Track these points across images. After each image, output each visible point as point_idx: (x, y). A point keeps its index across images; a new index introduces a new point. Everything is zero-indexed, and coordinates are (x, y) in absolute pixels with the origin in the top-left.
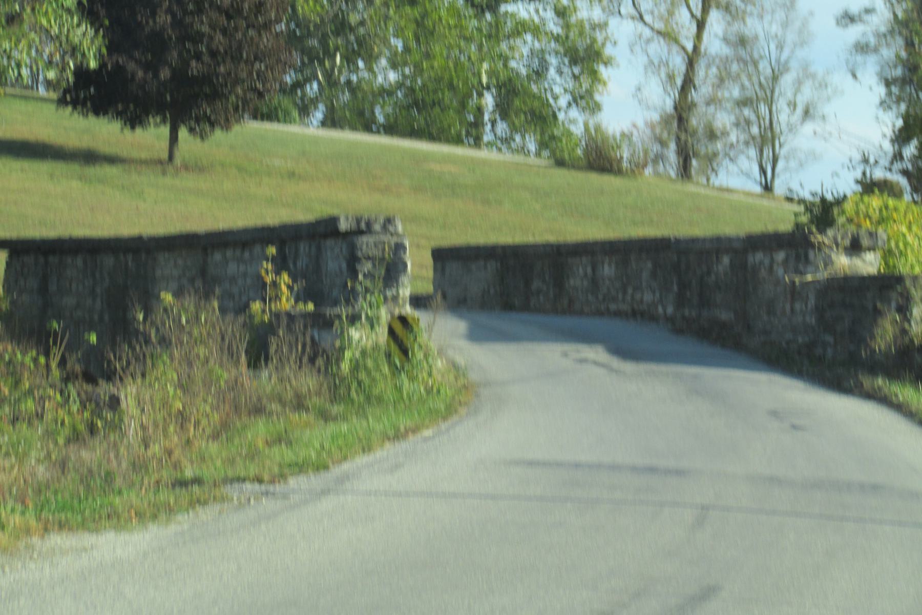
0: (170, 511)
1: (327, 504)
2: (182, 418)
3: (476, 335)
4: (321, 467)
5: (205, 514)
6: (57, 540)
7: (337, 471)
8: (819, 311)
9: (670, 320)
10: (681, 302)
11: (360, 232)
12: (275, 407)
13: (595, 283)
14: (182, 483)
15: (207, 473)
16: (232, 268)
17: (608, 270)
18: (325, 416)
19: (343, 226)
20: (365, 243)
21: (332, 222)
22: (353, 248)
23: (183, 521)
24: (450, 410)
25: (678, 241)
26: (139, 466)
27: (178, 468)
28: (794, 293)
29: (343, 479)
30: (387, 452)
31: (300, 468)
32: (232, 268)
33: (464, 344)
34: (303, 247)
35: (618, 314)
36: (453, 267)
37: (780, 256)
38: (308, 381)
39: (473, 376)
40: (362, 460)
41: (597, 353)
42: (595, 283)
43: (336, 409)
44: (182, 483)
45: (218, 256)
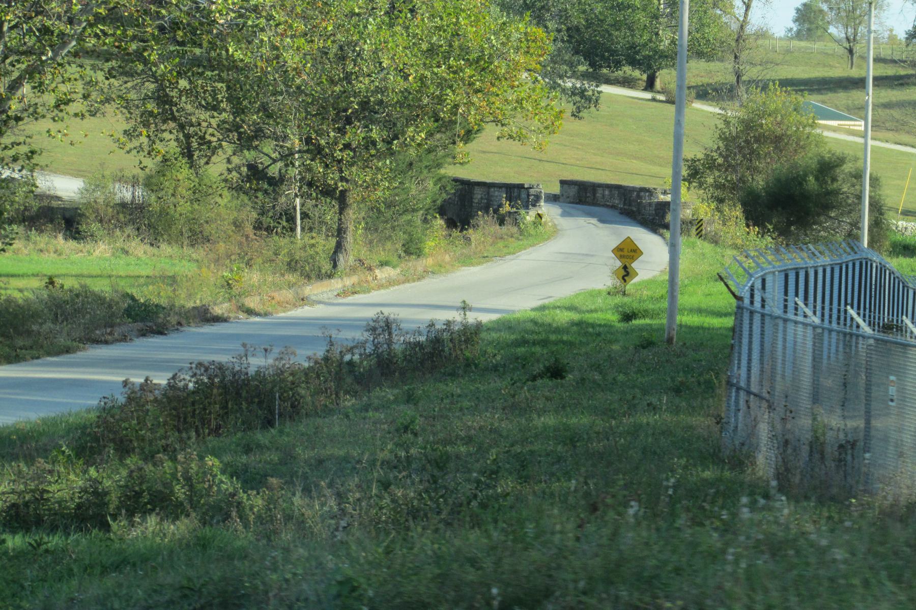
0: (483, 263)
1: (513, 262)
2: (483, 242)
3: (565, 214)
4: (514, 254)
5: (489, 264)
6: (463, 268)
7: (517, 254)
8: (655, 210)
9: (621, 209)
10: (625, 204)
11: (531, 188)
12: (506, 237)
13: (603, 195)
14: (484, 257)
15: (489, 255)
16: (496, 193)
17: (607, 192)
18: (518, 239)
19: (526, 186)
20: (532, 191)
21: (523, 185)
22: (528, 192)
23: (485, 265)
24: (549, 238)
25: (624, 186)
26: (475, 253)
27: (737, 335)
28: (650, 204)
29: (517, 257)
30: (530, 250)
31: (509, 254)
32: (496, 193)
33: (559, 217)
34: (516, 190)
35: (607, 206)
36: (566, 186)
37: (647, 194)
38: (515, 229)
39: (559, 227)
40: (523, 252)
41: (594, 221)
42: (603, 195)
43: (521, 237)
44: (484, 257)
45: (492, 190)
